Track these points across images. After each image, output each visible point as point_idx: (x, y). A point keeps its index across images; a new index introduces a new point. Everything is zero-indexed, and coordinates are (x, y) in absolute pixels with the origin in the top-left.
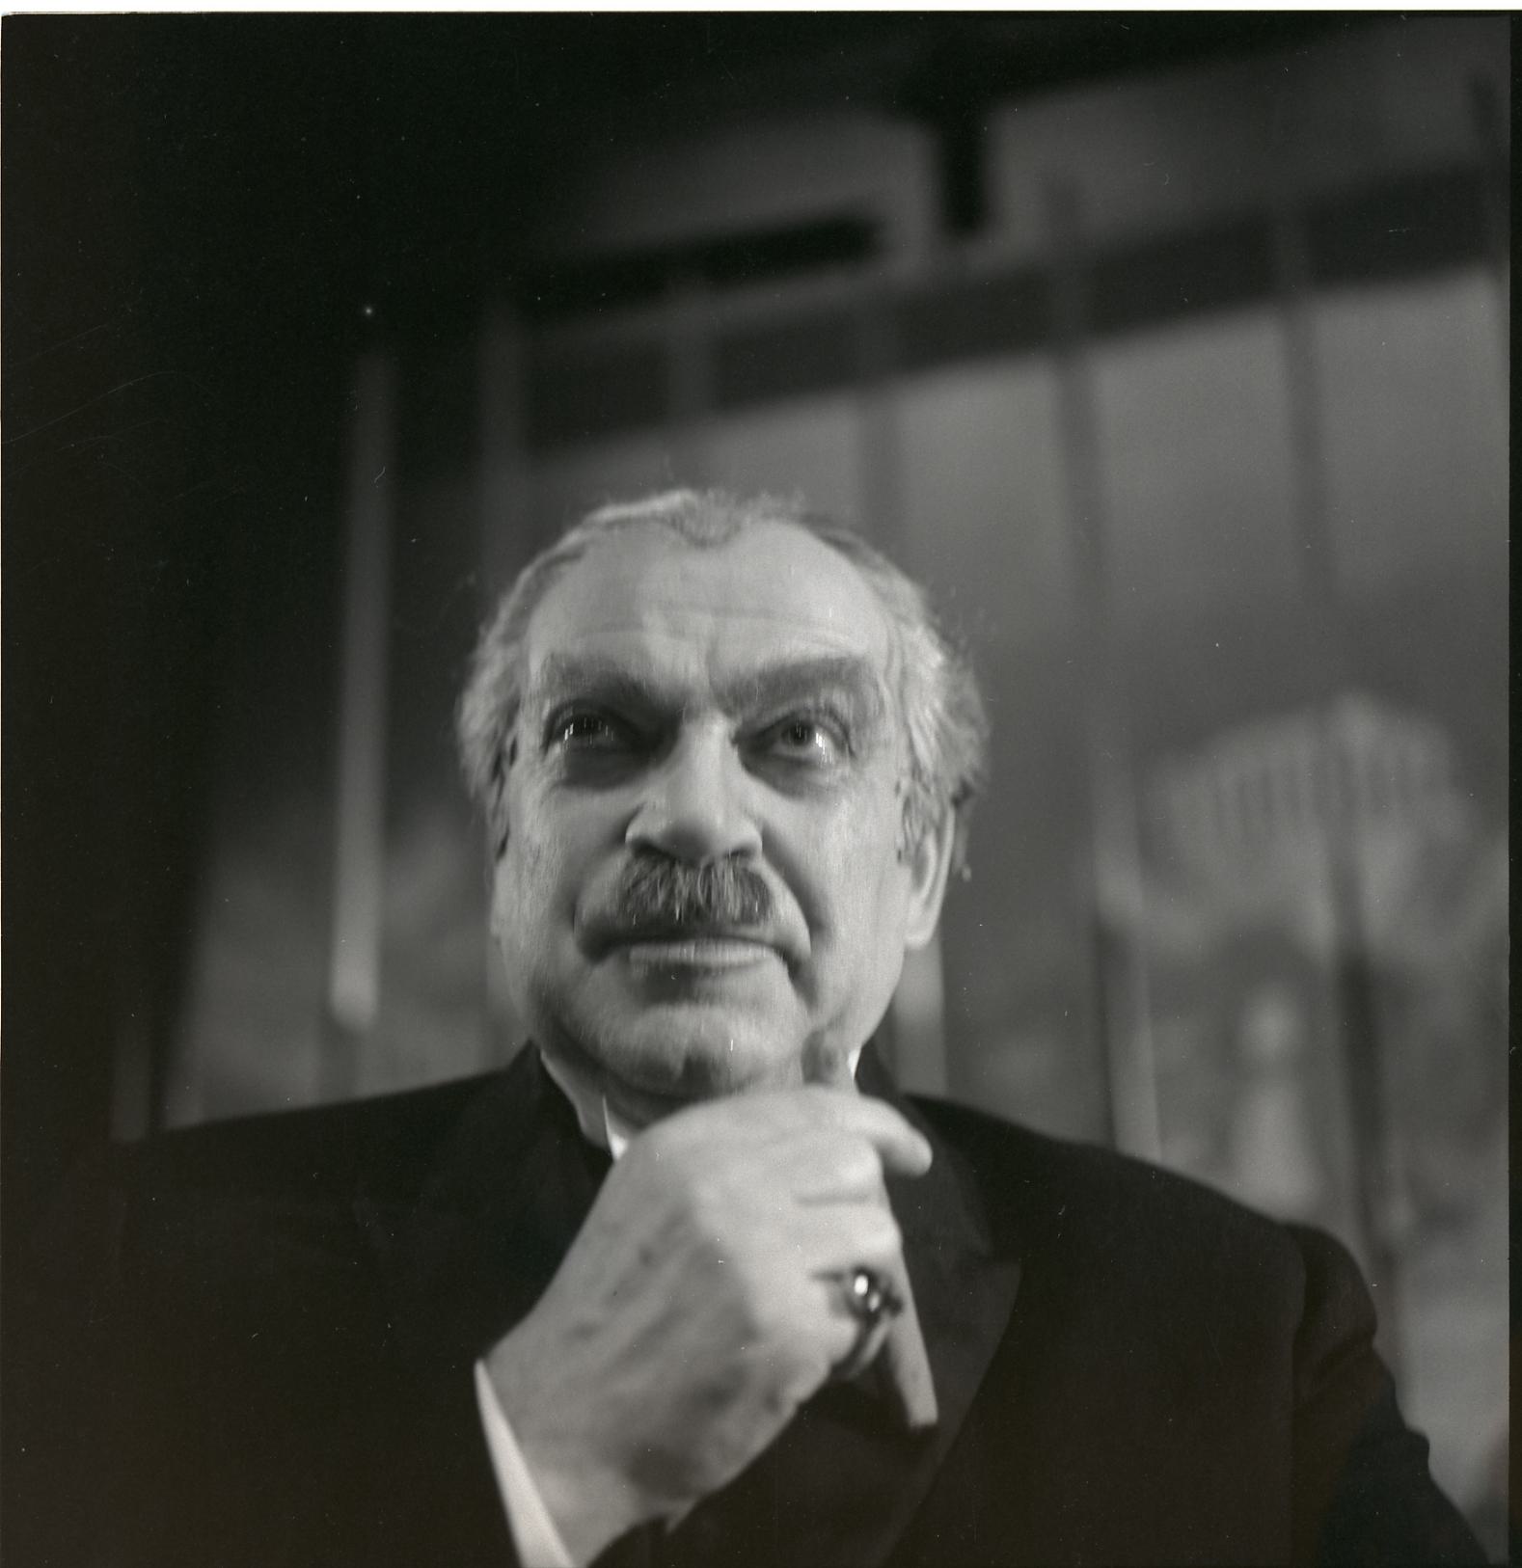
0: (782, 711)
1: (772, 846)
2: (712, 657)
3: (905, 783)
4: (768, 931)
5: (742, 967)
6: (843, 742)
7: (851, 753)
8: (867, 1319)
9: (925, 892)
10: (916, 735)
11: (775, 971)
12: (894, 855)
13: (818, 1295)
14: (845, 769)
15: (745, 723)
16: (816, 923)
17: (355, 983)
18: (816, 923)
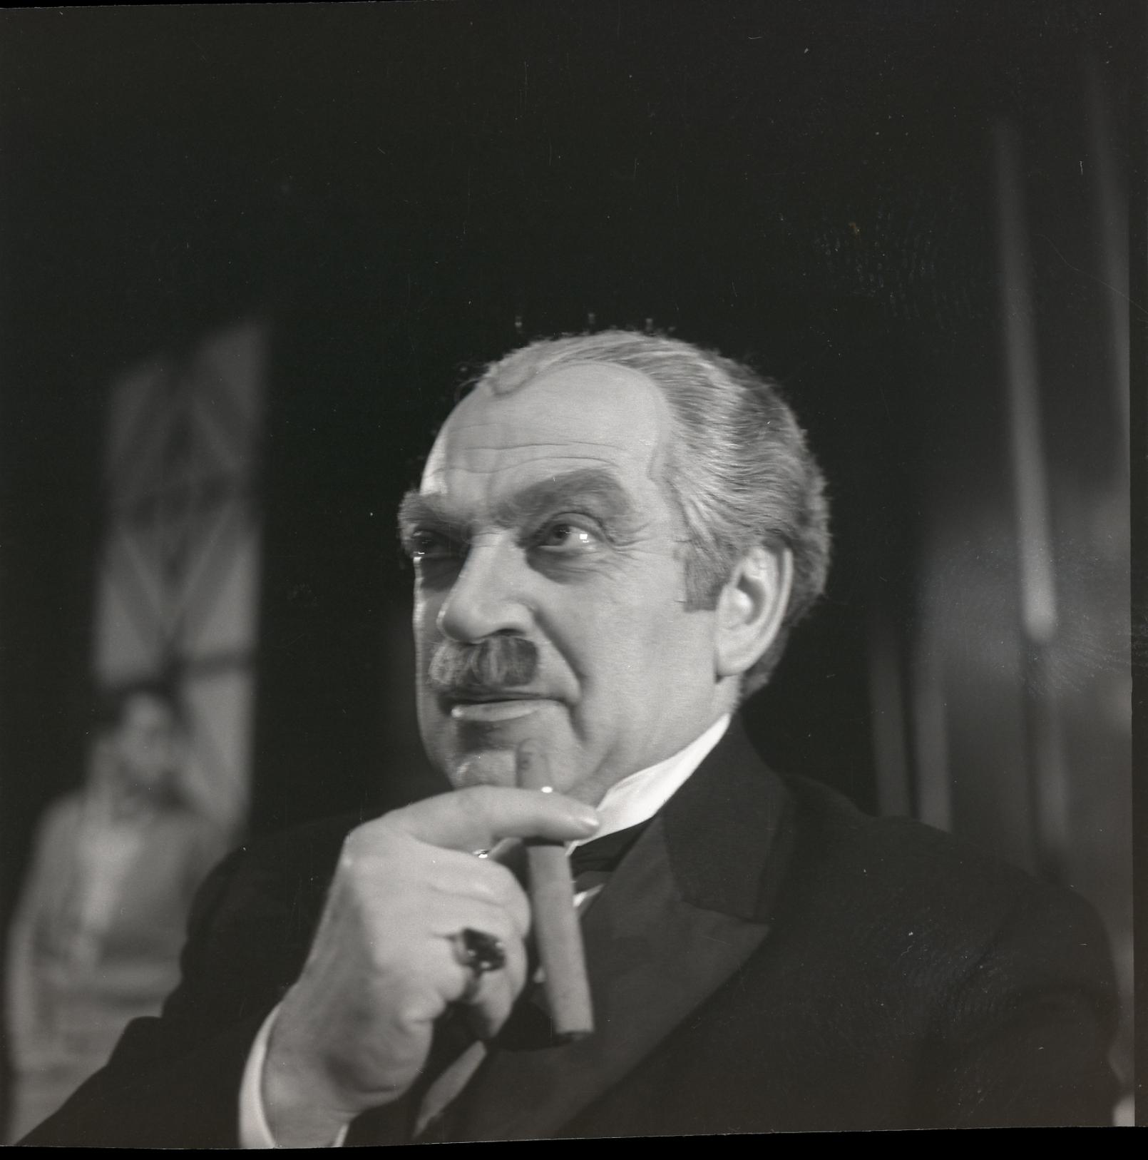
0: (545, 518)
1: (540, 618)
2: (490, 484)
3: (684, 550)
4: (540, 686)
5: (524, 718)
6: (602, 534)
7: (611, 540)
8: (475, 966)
9: (761, 621)
10: (691, 512)
11: (554, 714)
12: (679, 606)
13: (445, 948)
14: (606, 553)
15: (524, 529)
16: (581, 676)
17: (1040, 607)
18: (581, 676)
